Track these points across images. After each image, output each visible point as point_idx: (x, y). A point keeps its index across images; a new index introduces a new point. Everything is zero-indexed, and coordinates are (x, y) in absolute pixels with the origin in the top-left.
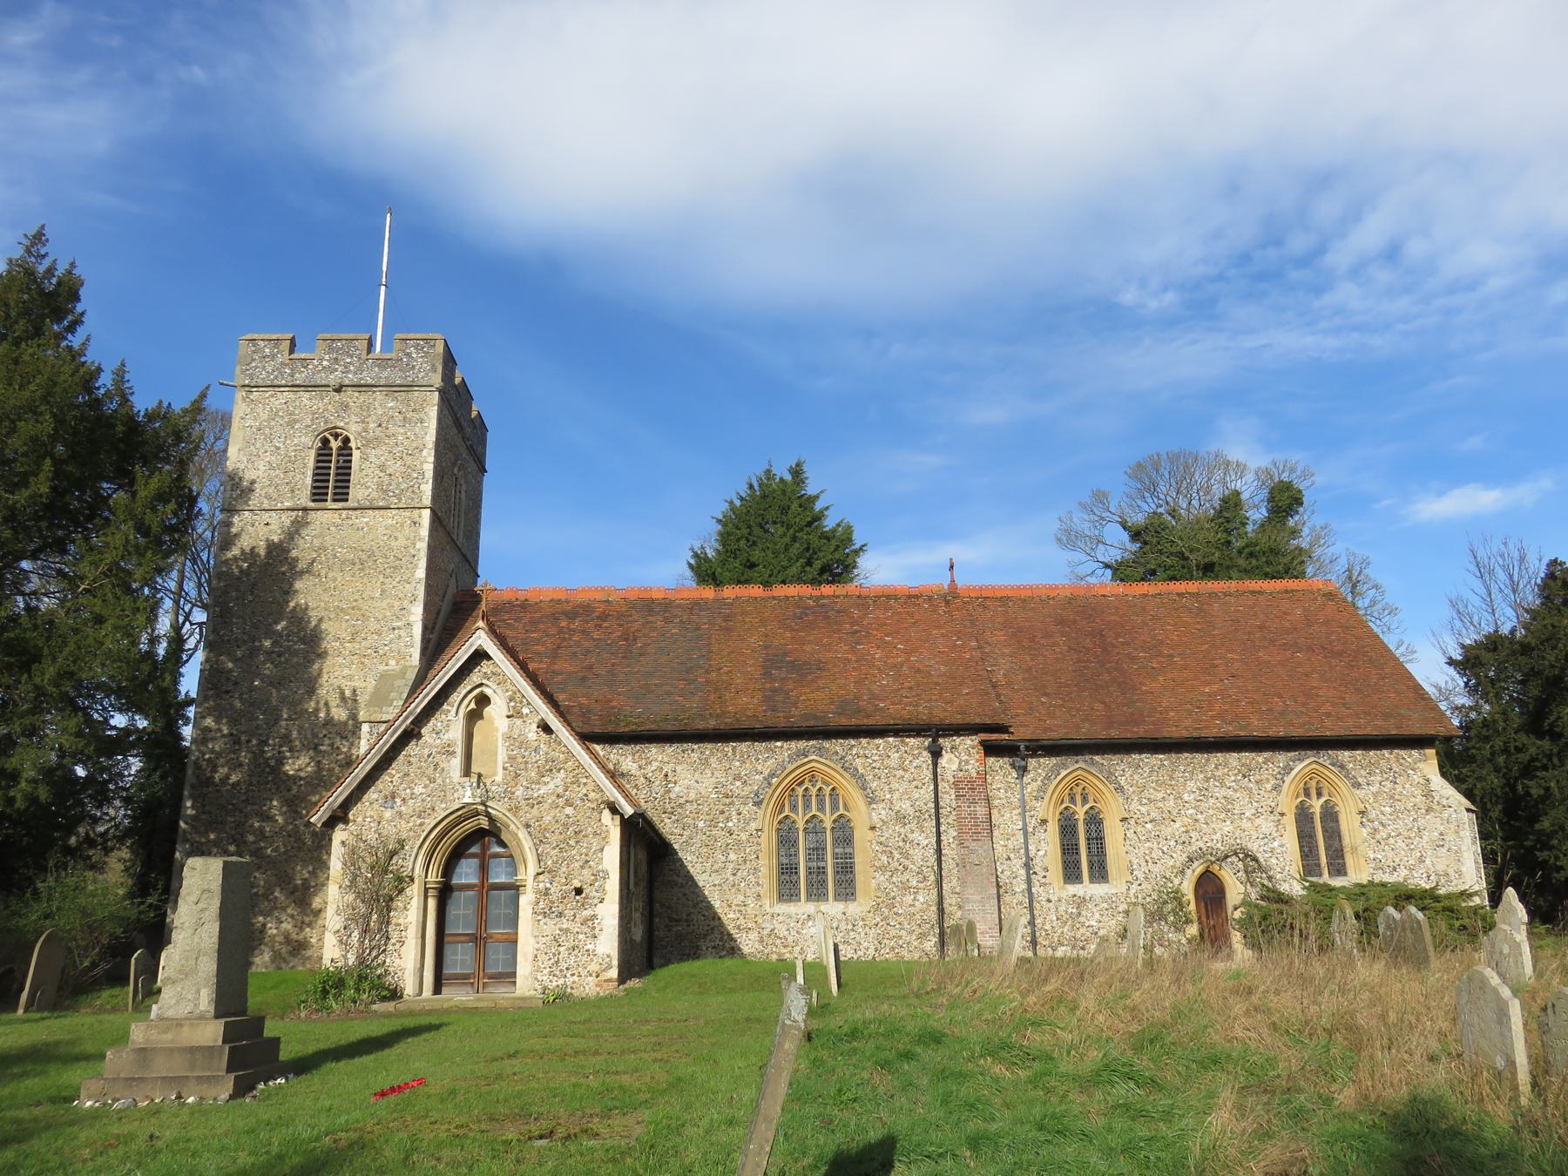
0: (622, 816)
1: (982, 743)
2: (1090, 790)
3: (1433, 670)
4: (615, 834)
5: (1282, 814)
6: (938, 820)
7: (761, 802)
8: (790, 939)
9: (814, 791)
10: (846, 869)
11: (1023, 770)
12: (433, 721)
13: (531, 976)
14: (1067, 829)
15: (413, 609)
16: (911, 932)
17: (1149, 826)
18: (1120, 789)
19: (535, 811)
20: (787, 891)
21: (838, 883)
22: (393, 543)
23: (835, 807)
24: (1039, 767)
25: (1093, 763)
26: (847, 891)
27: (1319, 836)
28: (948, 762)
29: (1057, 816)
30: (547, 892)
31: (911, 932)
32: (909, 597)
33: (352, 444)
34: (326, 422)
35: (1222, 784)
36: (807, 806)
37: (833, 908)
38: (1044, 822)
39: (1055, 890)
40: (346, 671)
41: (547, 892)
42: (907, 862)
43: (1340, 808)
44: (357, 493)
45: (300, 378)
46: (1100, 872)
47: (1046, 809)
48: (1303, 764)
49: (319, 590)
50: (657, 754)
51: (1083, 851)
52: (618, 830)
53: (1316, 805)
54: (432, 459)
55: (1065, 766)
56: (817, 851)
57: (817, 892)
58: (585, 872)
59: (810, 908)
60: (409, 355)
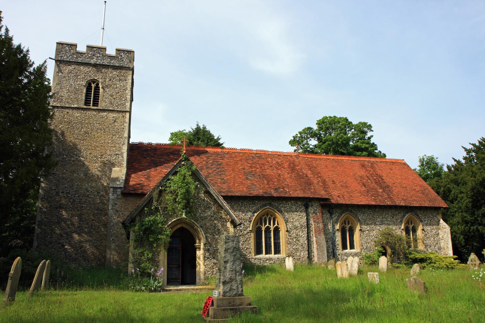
1: (320, 204)
12: (347, 203)
15: (124, 148)
17: (367, 232)
19: (204, 222)
23: (274, 224)
35: (387, 220)
44: (102, 105)
45: (80, 60)
56: (268, 238)
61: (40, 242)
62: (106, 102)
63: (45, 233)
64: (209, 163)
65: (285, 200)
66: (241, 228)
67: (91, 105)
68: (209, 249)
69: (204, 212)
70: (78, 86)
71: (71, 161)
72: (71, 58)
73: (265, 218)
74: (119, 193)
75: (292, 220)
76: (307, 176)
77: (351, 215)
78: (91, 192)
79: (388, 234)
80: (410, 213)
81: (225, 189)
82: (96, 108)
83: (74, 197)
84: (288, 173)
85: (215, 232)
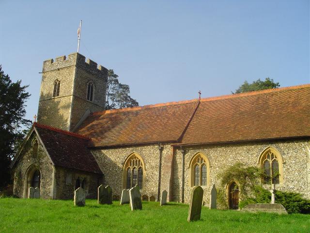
17: (217, 169)
44: (61, 94)
50: (111, 151)
55: (195, 152)
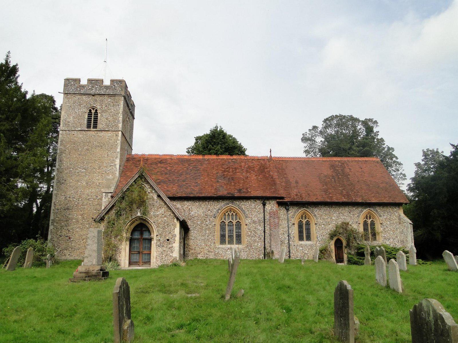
0: (180, 220)
2: (307, 216)
3: (404, 186)
4: (178, 225)
5: (359, 224)
6: (264, 223)
7: (216, 217)
8: (223, 255)
9: (230, 214)
10: (239, 236)
11: (288, 210)
13: (155, 262)
14: (300, 226)
16: (256, 253)
17: (323, 226)
18: (315, 215)
19: (156, 219)
20: (223, 241)
21: (237, 240)
22: (111, 142)
23: (236, 219)
24: (292, 211)
25: (308, 208)
26: (239, 241)
27: (370, 230)
28: (268, 207)
29: (298, 222)
30: (159, 240)
31: (256, 253)
32: (258, 159)
33: (98, 112)
34: (90, 105)
36: (229, 218)
37: (235, 246)
38: (294, 224)
39: (295, 241)
40: (97, 178)
41: (159, 240)
42: (256, 234)
43: (376, 222)
44: (100, 126)
45: (82, 92)
46: (309, 238)
47: (296, 221)
48: (366, 211)
49: (89, 154)
51: (304, 232)
52: (179, 224)
53: (369, 221)
54: (121, 117)
57: (231, 242)
58: (170, 235)
59: (229, 246)
60: (114, 85)
61: (53, 236)
62: (103, 125)
63: (57, 229)
64: (189, 169)
65: (245, 199)
66: (207, 223)
67: (92, 127)
68: (159, 239)
69: (157, 211)
70: (81, 113)
71: (76, 173)
72: (75, 91)
73: (229, 214)
74: (110, 197)
75: (251, 216)
76: (272, 178)
77: (308, 211)
78: (91, 196)
79: (345, 225)
80: (368, 209)
81: (196, 191)
82: (95, 129)
83: (78, 201)
84: (256, 175)
85: (164, 227)
